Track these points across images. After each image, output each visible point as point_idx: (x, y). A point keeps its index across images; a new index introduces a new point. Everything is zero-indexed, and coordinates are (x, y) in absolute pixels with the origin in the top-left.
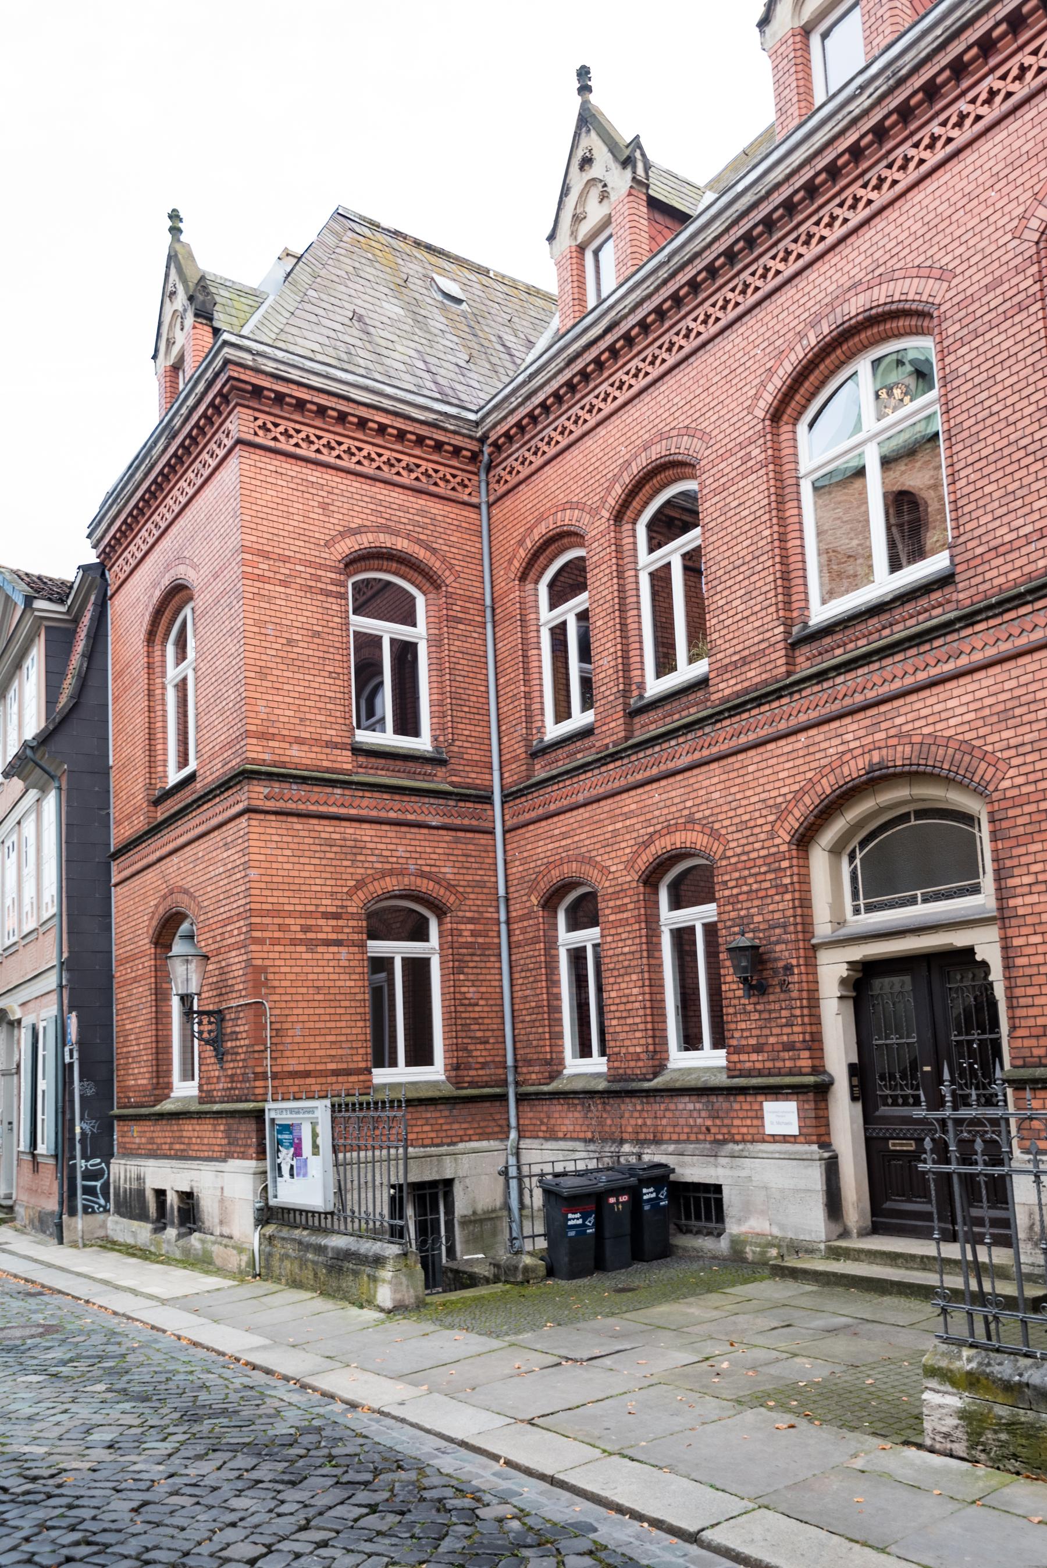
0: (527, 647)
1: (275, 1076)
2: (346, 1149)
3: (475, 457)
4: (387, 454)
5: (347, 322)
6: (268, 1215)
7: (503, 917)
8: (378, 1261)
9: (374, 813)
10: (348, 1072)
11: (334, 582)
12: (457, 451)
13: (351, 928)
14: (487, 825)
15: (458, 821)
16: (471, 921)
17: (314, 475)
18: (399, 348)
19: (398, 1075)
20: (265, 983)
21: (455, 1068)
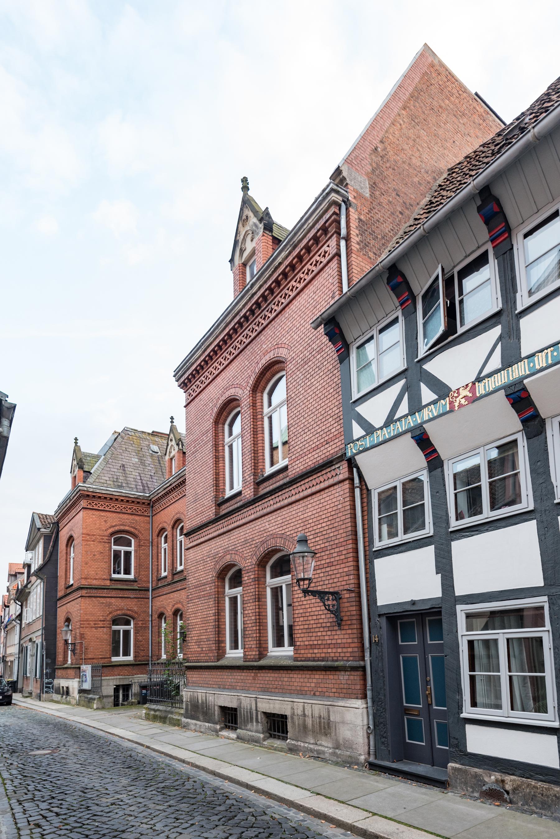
0: (158, 553)
1: (85, 659)
2: (95, 676)
3: (149, 504)
4: (124, 506)
5: (119, 468)
6: (81, 691)
7: (150, 619)
8: (94, 699)
9: (115, 595)
10: (105, 658)
11: (107, 539)
12: (144, 503)
13: (107, 624)
14: (147, 596)
15: (139, 596)
16: (141, 621)
17: (103, 514)
18: (133, 473)
19: (121, 658)
20: (84, 638)
21: (135, 657)
